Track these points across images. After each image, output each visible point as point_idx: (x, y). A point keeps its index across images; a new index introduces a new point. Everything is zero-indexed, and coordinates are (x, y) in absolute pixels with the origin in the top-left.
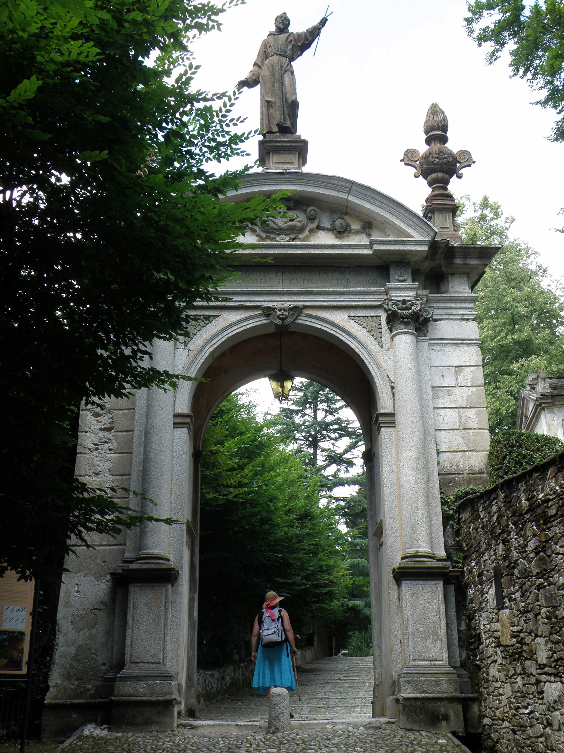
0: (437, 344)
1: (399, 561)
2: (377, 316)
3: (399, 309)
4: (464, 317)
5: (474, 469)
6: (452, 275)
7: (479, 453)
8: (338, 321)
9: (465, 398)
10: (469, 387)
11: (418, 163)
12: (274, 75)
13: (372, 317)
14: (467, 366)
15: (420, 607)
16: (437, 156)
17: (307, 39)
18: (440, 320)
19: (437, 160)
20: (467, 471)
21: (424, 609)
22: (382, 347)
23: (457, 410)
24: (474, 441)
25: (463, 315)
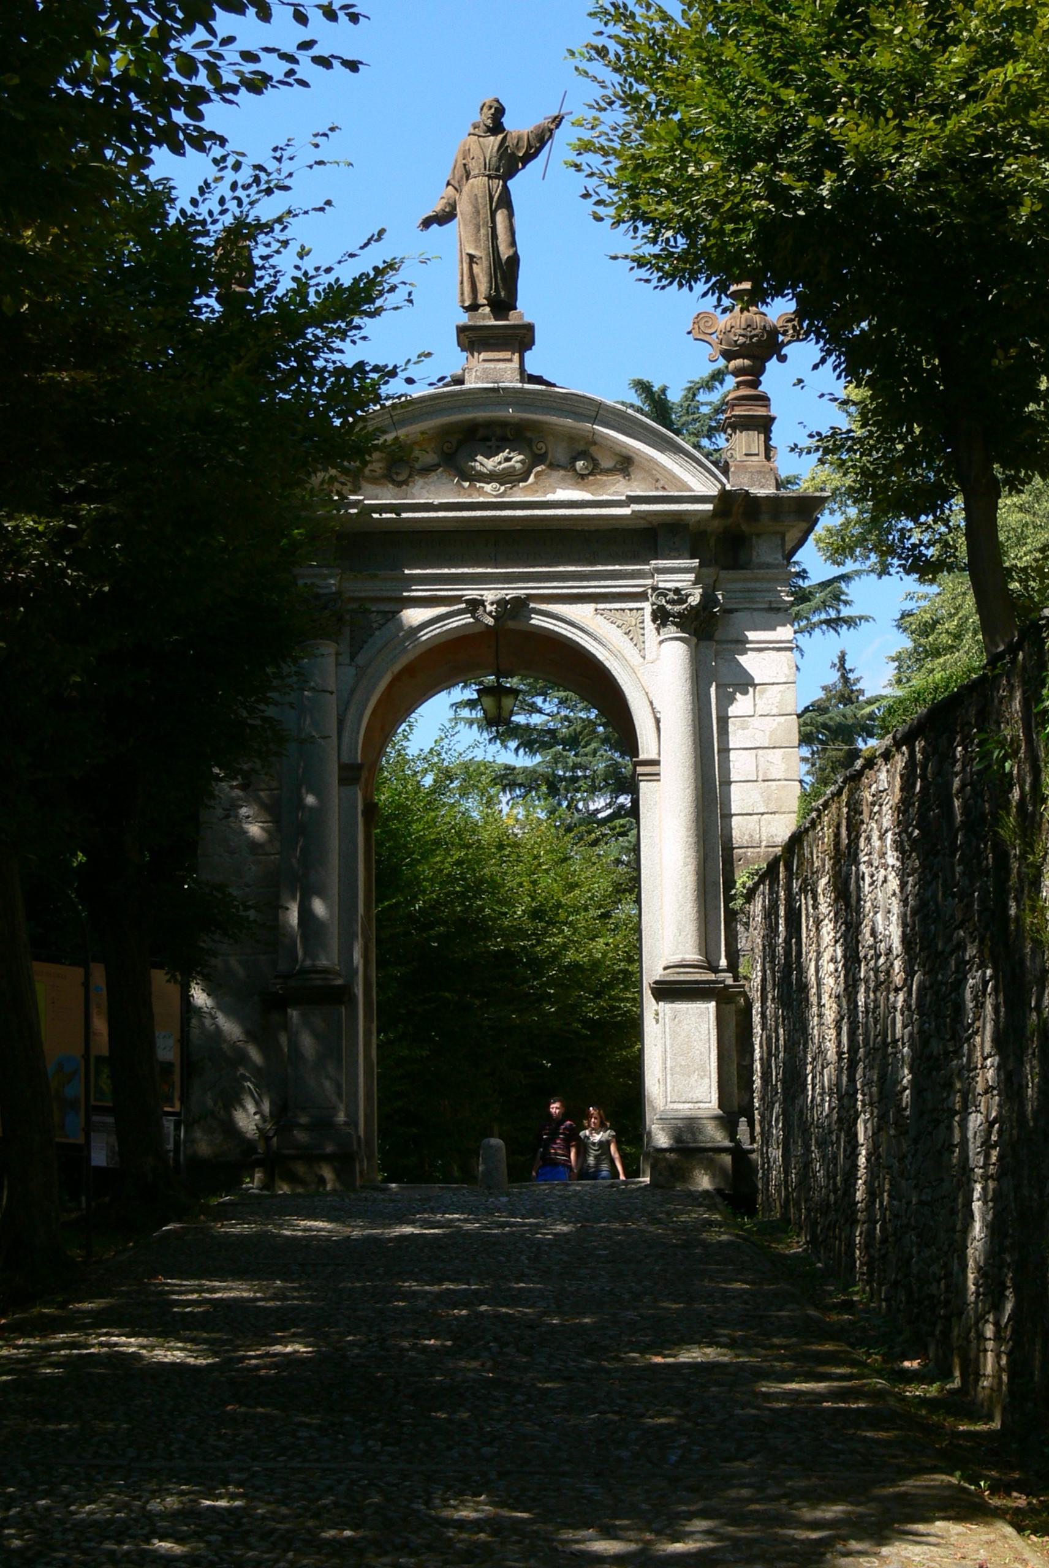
1: (661, 971)
2: (638, 609)
3: (667, 602)
5: (775, 839)
6: (758, 535)
7: (783, 816)
8: (578, 618)
9: (768, 733)
11: (714, 336)
12: (478, 212)
13: (631, 610)
14: (773, 684)
15: (683, 1034)
16: (743, 332)
17: (530, 146)
18: (737, 610)
19: (742, 340)
20: (764, 844)
21: (688, 1036)
22: (644, 658)
24: (777, 799)
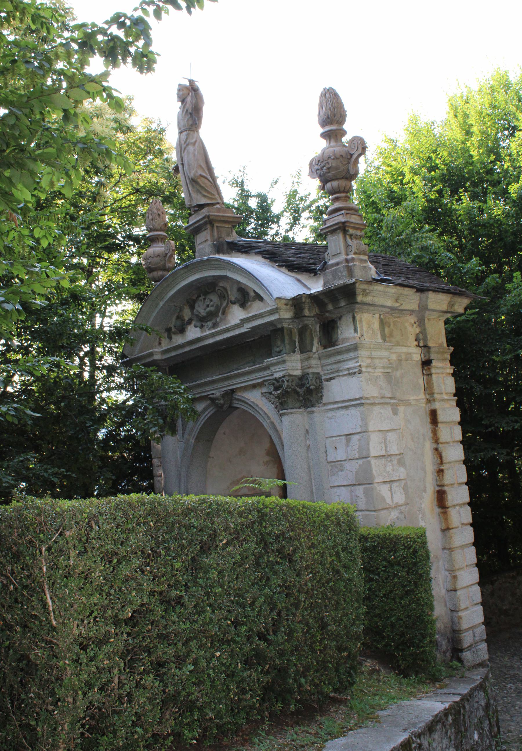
0: (331, 410)
4: (351, 371)
10: (357, 459)
23: (348, 488)
25: (348, 369)
